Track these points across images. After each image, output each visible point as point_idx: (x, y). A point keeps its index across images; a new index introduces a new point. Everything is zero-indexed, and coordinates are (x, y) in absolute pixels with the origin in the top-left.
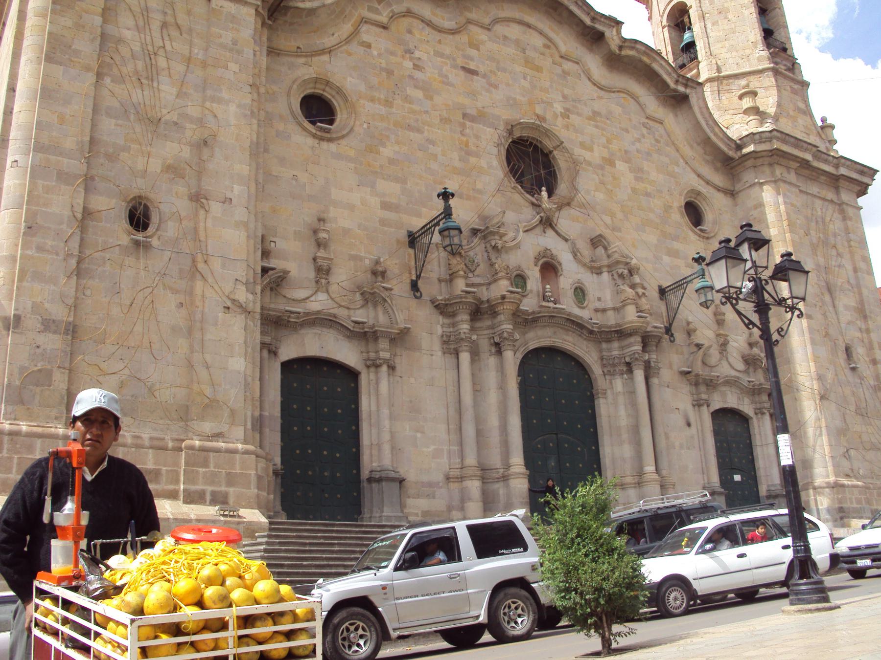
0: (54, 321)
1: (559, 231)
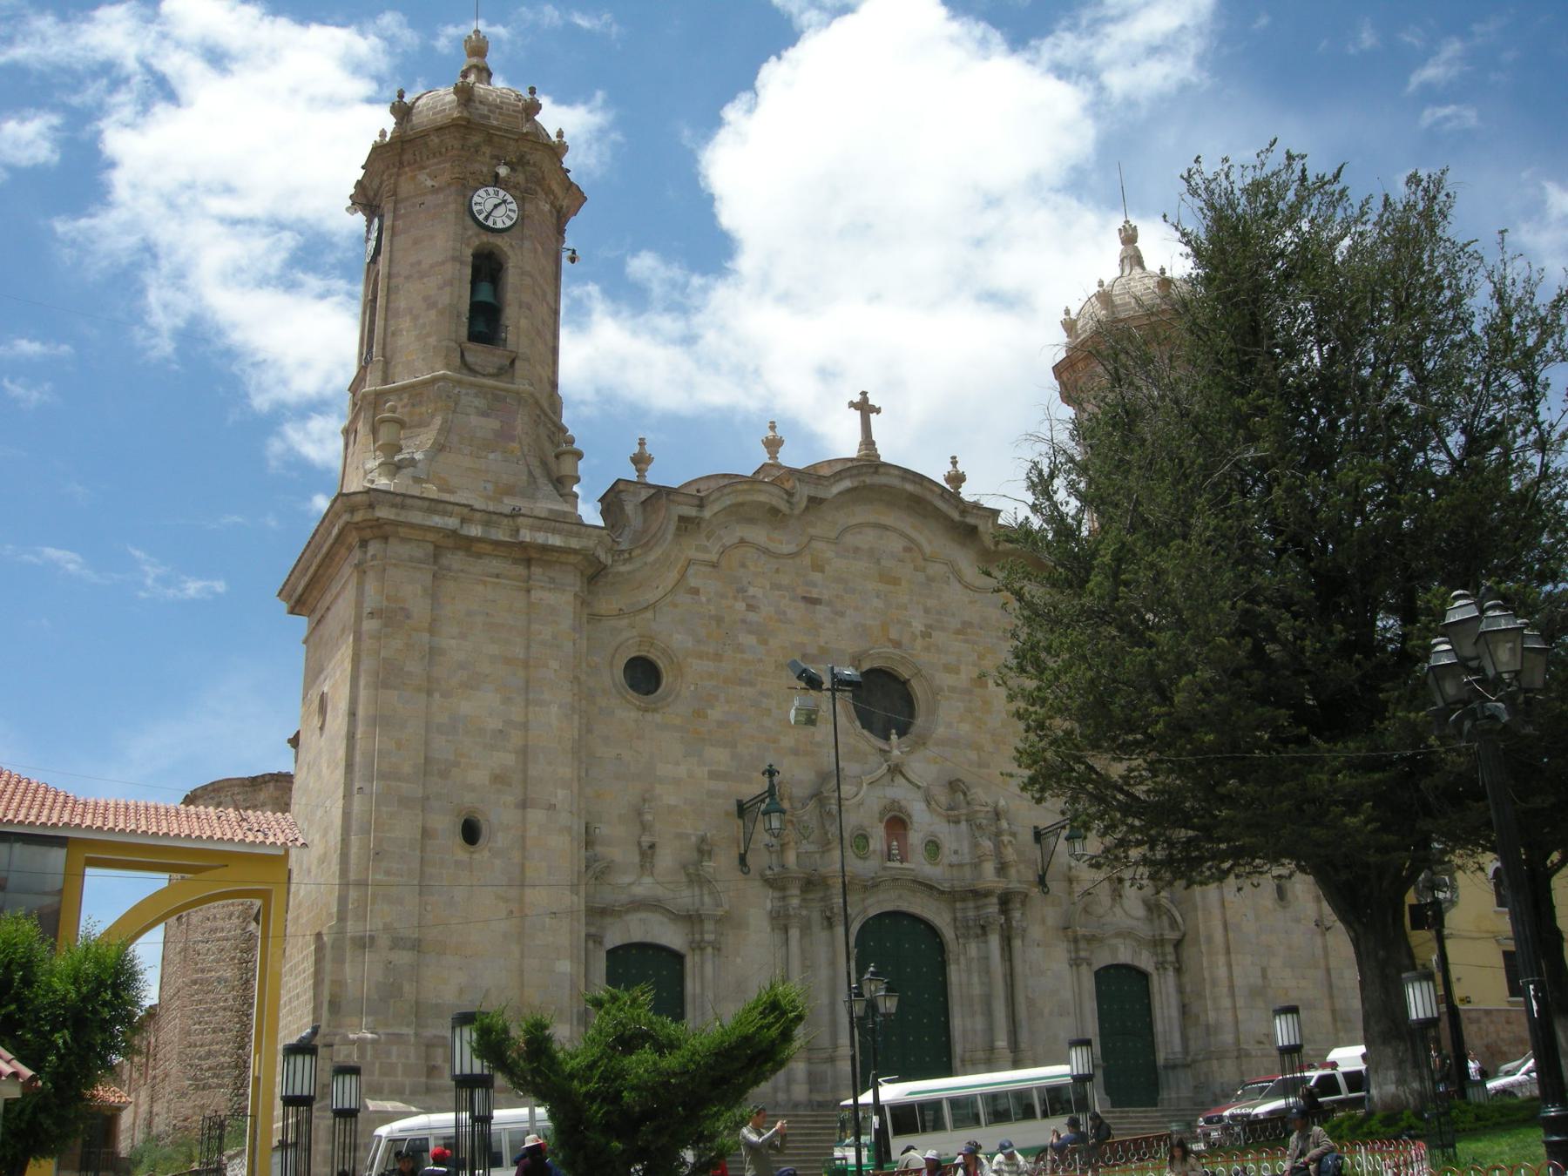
0: (402, 939)
1: (908, 776)
